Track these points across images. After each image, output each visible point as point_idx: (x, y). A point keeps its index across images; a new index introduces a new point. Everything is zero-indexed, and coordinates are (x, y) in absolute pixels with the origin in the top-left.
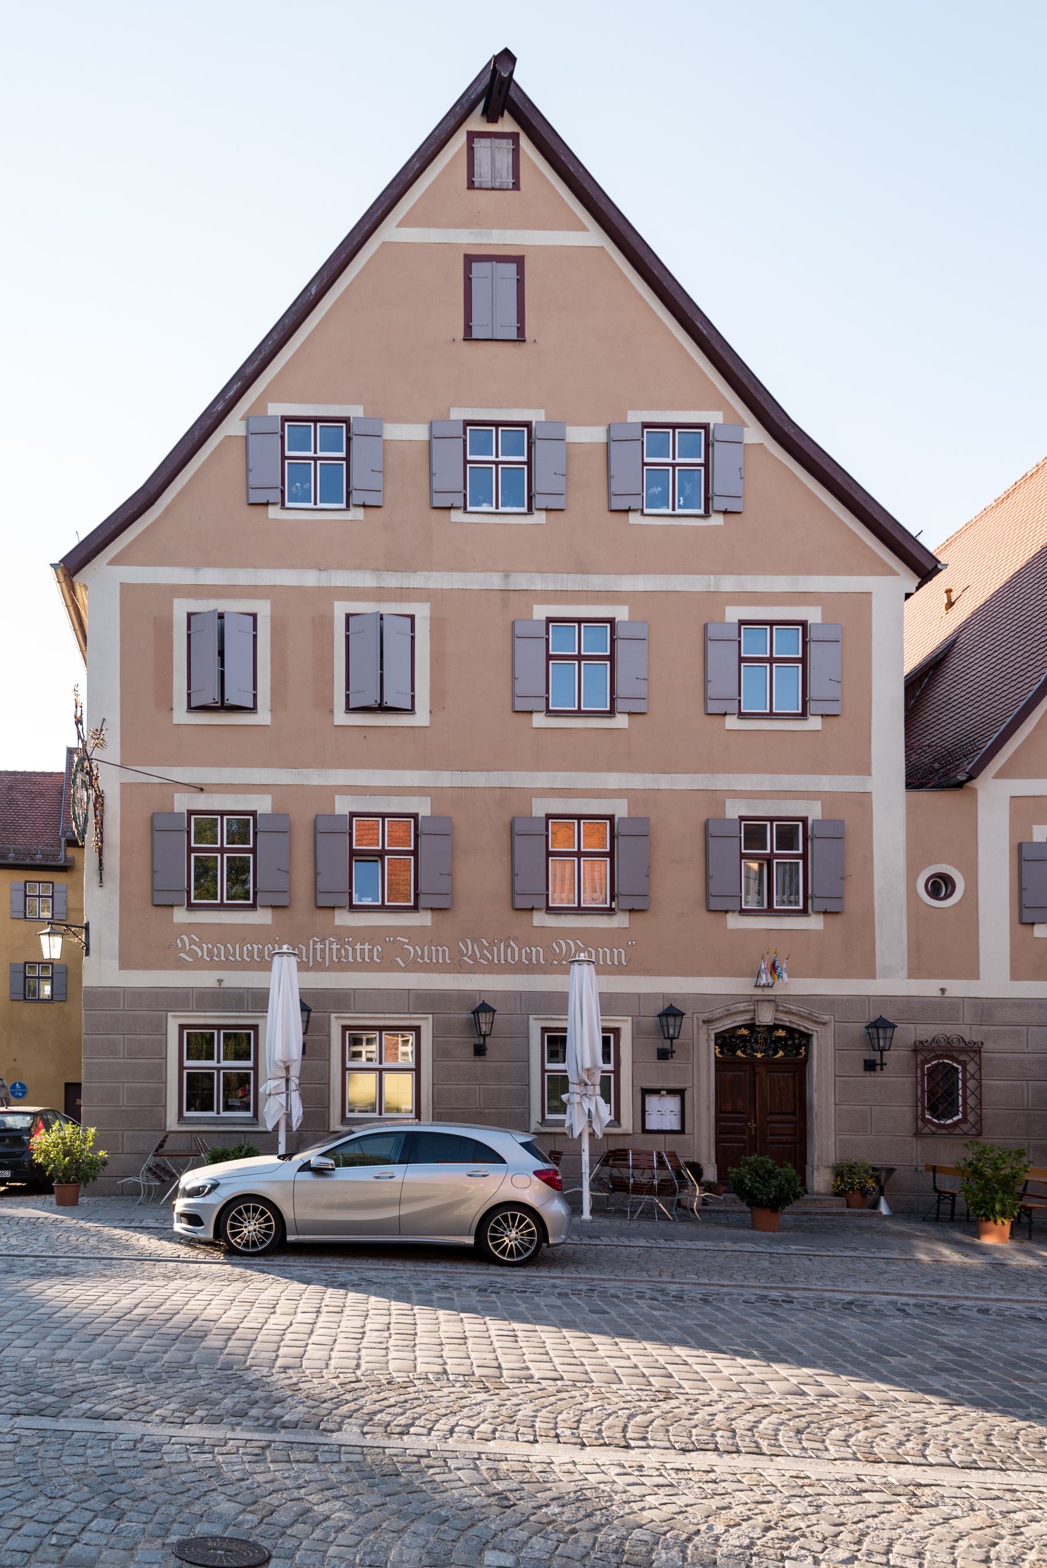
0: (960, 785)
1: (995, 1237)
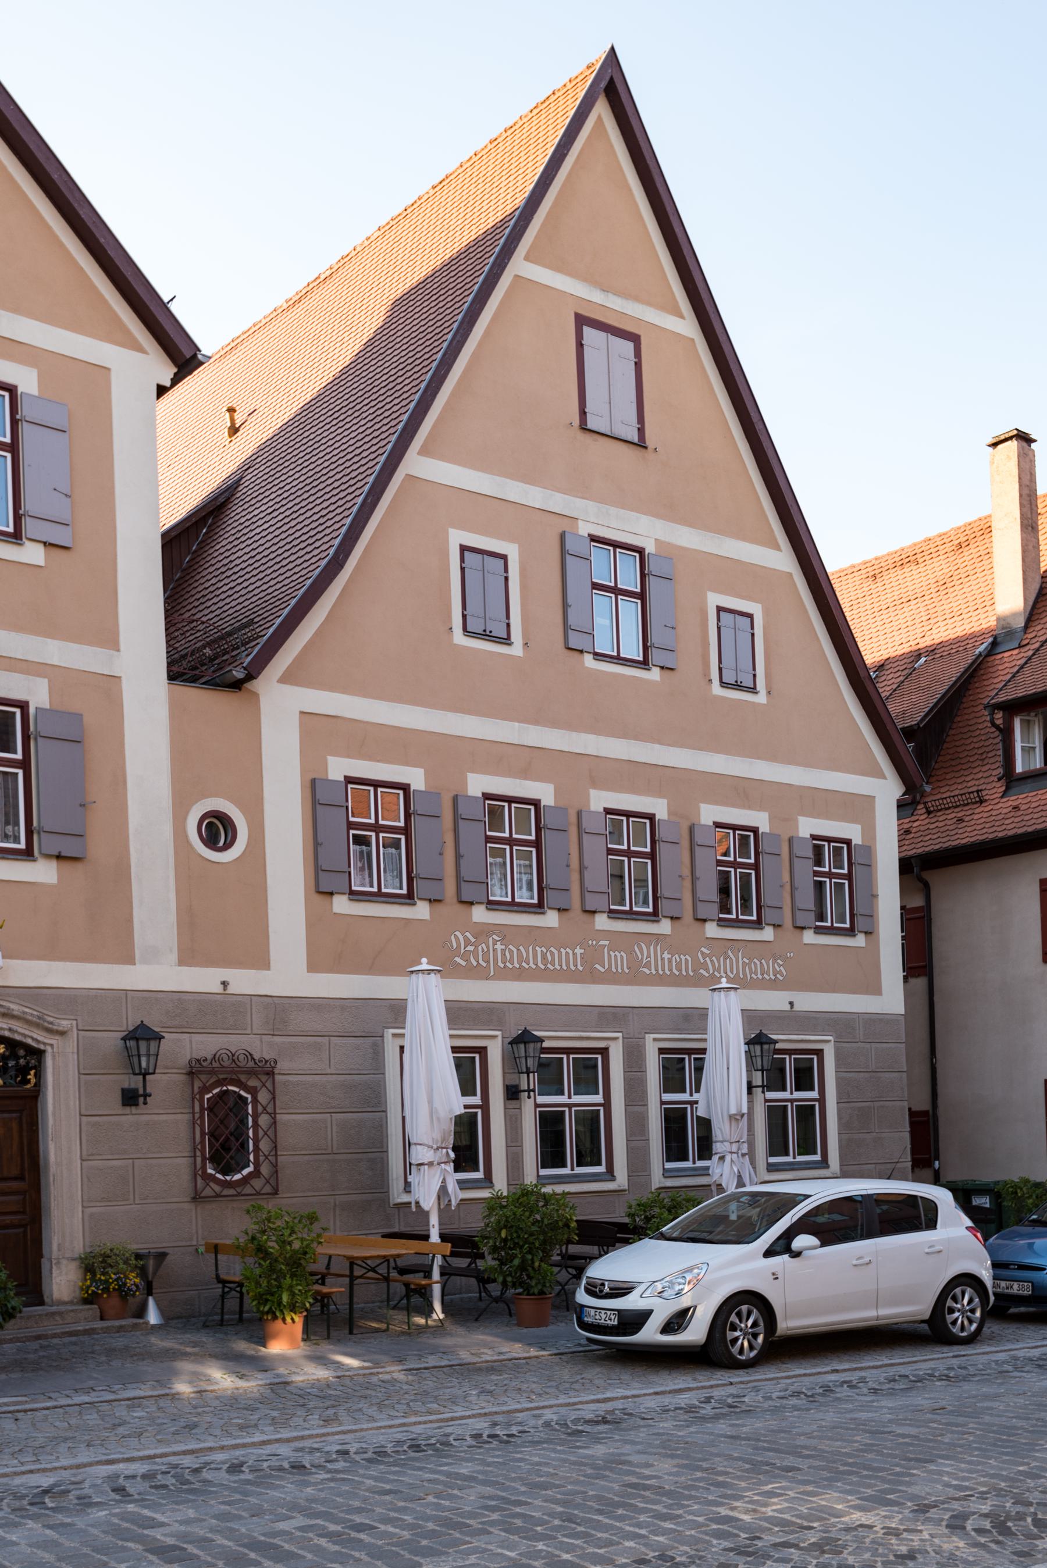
0: (237, 685)
1: (285, 1343)
